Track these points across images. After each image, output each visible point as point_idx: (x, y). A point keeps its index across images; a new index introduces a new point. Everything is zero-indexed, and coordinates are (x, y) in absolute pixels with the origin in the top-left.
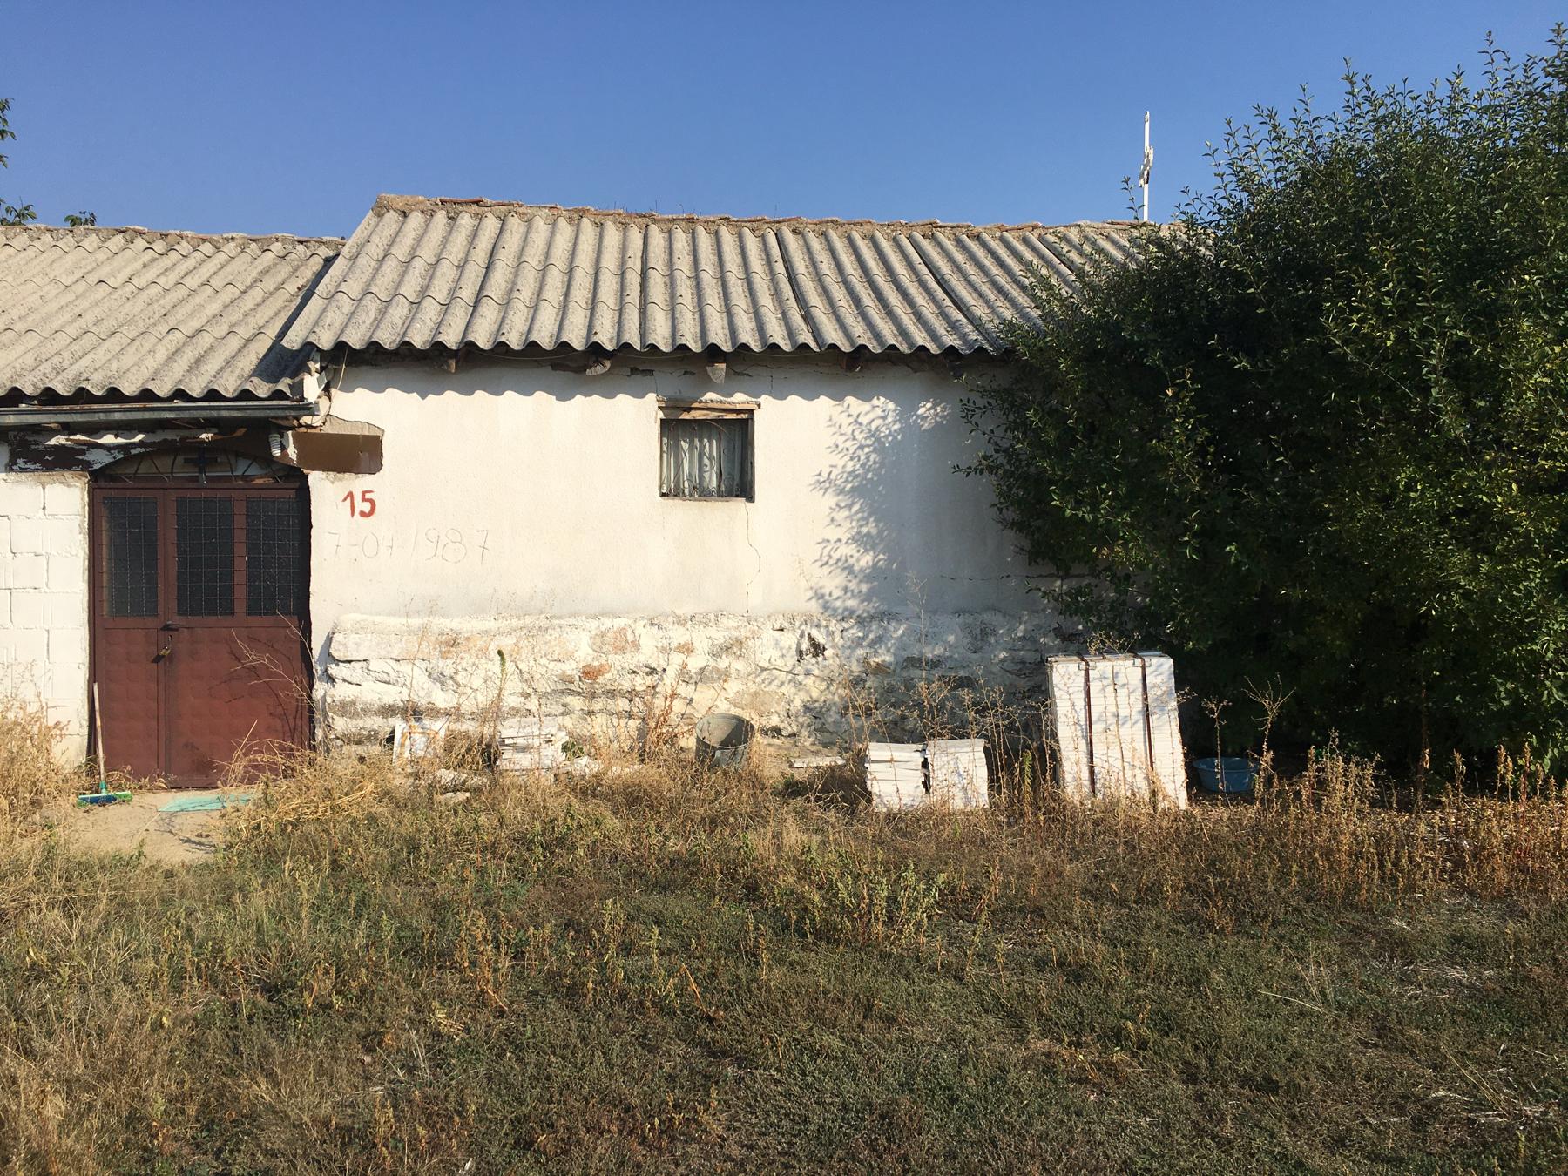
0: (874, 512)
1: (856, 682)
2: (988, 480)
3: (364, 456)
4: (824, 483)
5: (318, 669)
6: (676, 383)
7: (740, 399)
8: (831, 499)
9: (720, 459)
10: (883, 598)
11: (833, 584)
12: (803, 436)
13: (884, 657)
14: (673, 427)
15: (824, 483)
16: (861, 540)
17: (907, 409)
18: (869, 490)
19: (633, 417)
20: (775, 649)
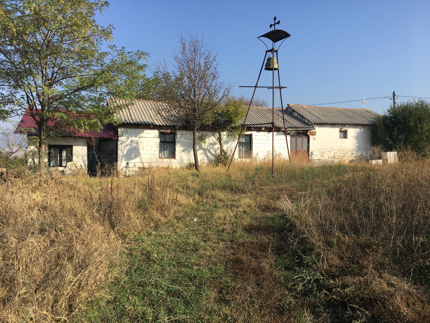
0: (358, 140)
1: (356, 157)
2: (406, 104)
3: (166, 153)
4: (353, 137)
5: (310, 155)
6: (341, 126)
7: (346, 129)
8: (354, 139)
9: (344, 135)
10: (359, 148)
11: (354, 147)
12: (352, 132)
13: (359, 155)
14: (340, 131)
15: (353, 137)
16: (357, 143)
17: (360, 130)
18: (357, 138)
19: (336, 130)
20: (349, 154)
